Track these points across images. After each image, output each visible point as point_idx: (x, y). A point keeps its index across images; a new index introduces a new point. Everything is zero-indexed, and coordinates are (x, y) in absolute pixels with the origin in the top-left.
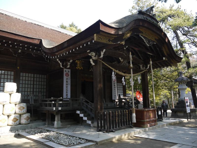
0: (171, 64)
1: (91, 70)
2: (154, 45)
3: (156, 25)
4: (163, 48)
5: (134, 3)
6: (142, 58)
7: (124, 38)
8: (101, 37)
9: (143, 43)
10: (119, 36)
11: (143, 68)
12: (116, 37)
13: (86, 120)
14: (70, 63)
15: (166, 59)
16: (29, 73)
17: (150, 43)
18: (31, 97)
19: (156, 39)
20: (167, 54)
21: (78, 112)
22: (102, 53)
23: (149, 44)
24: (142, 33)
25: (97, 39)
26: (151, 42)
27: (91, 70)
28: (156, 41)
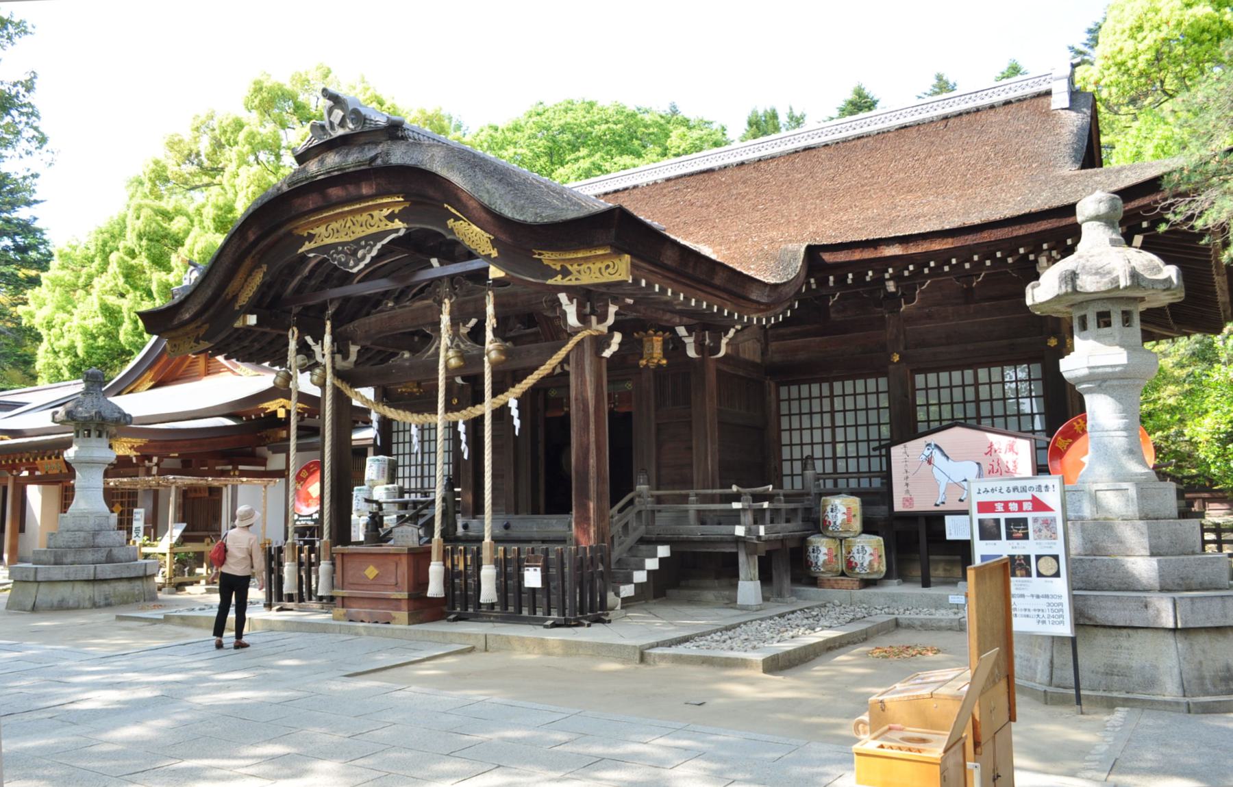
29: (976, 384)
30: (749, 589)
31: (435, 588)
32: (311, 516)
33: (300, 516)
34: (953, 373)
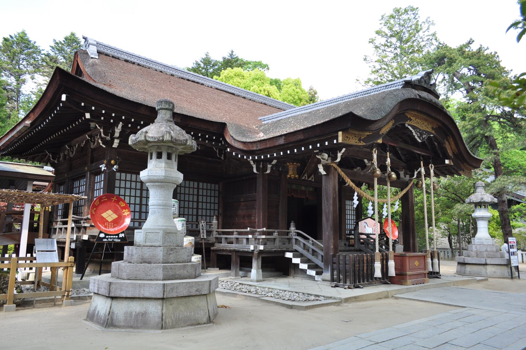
0: (460, 172)
1: (304, 178)
2: (429, 138)
3: (435, 105)
4: (447, 143)
5: (381, 24)
6: (403, 158)
7: (381, 133)
8: (349, 136)
9: (409, 133)
10: (375, 132)
11: (405, 176)
12: (371, 133)
13: (308, 270)
14: (271, 164)
15: (450, 162)
16: (211, 183)
17: (422, 138)
18: (202, 226)
19: (434, 127)
20: (453, 153)
21: (289, 255)
22: (339, 155)
23: (421, 138)
24: (411, 120)
25: (343, 140)
26: (425, 134)
27: (304, 178)
28: (433, 132)
29: (198, 188)
30: (255, 272)
31: (392, 272)
32: (118, 235)
33: (106, 235)
34: (191, 182)
